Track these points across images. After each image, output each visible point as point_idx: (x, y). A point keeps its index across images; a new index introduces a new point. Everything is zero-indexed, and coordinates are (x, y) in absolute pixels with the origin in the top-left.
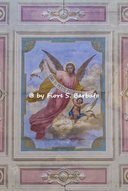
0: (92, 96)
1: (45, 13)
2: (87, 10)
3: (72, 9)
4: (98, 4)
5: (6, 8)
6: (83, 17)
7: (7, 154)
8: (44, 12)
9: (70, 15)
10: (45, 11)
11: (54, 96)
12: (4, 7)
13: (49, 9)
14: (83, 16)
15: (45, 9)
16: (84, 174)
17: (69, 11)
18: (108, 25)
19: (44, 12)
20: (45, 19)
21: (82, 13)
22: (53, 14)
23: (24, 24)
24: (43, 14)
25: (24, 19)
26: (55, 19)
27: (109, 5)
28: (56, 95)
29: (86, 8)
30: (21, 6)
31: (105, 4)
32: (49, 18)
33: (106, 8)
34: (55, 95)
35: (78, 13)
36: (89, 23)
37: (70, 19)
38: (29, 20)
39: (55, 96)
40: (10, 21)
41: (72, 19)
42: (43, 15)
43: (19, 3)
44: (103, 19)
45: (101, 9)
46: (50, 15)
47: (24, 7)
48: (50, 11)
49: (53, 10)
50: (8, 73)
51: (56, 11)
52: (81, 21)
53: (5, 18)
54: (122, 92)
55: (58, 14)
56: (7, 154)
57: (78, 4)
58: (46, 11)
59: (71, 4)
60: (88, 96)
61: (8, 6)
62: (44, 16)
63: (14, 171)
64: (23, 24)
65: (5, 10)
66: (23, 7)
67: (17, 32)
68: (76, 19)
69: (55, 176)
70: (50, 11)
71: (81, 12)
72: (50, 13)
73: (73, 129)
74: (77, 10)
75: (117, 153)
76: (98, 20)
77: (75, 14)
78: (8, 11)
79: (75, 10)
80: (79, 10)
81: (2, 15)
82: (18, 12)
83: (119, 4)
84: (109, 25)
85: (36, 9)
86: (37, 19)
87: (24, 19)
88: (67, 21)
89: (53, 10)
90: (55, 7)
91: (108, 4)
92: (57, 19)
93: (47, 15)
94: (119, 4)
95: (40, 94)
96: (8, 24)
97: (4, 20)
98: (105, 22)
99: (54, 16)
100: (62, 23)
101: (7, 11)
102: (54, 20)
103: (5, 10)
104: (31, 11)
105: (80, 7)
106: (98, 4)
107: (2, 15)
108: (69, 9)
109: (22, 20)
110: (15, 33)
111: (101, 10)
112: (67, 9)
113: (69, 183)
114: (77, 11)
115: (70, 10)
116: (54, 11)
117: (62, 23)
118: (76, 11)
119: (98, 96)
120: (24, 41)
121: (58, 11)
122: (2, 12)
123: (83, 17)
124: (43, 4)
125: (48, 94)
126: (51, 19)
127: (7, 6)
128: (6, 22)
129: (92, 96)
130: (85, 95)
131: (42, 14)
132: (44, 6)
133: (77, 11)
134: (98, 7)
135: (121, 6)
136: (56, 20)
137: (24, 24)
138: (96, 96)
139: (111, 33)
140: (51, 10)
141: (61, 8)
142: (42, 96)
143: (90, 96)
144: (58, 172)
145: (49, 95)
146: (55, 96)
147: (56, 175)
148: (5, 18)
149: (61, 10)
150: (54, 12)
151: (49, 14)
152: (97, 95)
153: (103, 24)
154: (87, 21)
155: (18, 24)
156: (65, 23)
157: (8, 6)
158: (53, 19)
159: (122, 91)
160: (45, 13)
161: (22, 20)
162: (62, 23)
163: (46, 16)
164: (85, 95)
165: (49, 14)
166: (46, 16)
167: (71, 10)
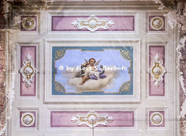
0: (120, 69)
1: (74, 118)
2: (116, 116)
3: (101, 114)
4: (126, 109)
5: (35, 113)
6: (112, 122)
7: (39, 97)
8: (73, 117)
9: (99, 120)
10: (74, 116)
11: (83, 69)
12: (34, 113)
13: (78, 115)
14: (112, 121)
15: (74, 114)
16: (111, 117)
17: (98, 116)
18: (136, 130)
19: (73, 117)
20: (74, 124)
21: (110, 118)
22: (82, 119)
23: (54, 130)
24: (72, 119)
25: (53, 124)
26: (83, 124)
27: (137, 110)
28: (85, 68)
29: (115, 113)
30: (51, 112)
31: (133, 109)
32: (79, 124)
33: (134, 113)
34: (84, 67)
35: (107, 118)
36: (117, 129)
37: (99, 124)
38: (59, 126)
39: (84, 69)
40: (40, 127)
41: (101, 124)
42: (72, 121)
43: (48, 109)
44: (132, 124)
45: (129, 114)
46: (79, 120)
47: (54, 113)
48: (79, 116)
49: (83, 115)
50: (39, 59)
51: (84, 116)
52: (109, 126)
53: (34, 124)
54: (150, 69)
55: (87, 119)
56: (39, 97)
57: (107, 109)
58: (75, 117)
59: (100, 109)
60: (117, 69)
61: (38, 111)
62: (73, 121)
63: (45, 113)
64: (52, 130)
65: (35, 116)
66: (53, 112)
67: (48, 41)
68: (105, 124)
69: (84, 119)
70: (79, 116)
71: (110, 117)
72: (79, 118)
73: (101, 89)
74: (105, 115)
75: (143, 97)
76: (126, 125)
77: (103, 119)
78: (38, 117)
79: (103, 115)
80: (108, 115)
81: (32, 120)
82: (48, 118)
83: (147, 109)
84: (137, 130)
85: (65, 114)
86: (66, 124)
87: (53, 124)
88: (95, 126)
89: (81, 115)
90: (84, 112)
91: (136, 109)
92: (86, 124)
93: (76, 121)
94: (147, 109)
95: (70, 66)
96: (38, 129)
97: (34, 126)
98: (133, 127)
99: (83, 121)
100: (90, 128)
101: (36, 116)
102: (83, 125)
103: (35, 116)
104: (60, 116)
105: (108, 112)
106: (126, 109)
107: (32, 120)
108: (98, 114)
109: (52, 126)
110: (46, 42)
111: (130, 116)
112: (96, 115)
113: (97, 126)
114: (106, 116)
115: (98, 115)
116: (82, 116)
117: (90, 128)
118: (105, 117)
119: (125, 69)
120: (55, 49)
121: (87, 116)
122: (32, 117)
123: (112, 122)
124: (72, 109)
125: (77, 66)
126: (80, 124)
127: (36, 111)
128: (36, 128)
129: (120, 69)
130: (113, 67)
131: (71, 119)
132: (73, 111)
133: (106, 116)
134: (126, 112)
135: (149, 111)
136: (85, 126)
137: (54, 130)
138: (124, 69)
139: (139, 42)
140: (80, 116)
141: (90, 114)
142: (72, 68)
143: (118, 68)
144: (86, 115)
145: (78, 67)
146: (84, 69)
147: (85, 118)
148: (34, 124)
149: (90, 115)
150: (83, 118)
151: (78, 119)
152: (125, 68)
153: (131, 129)
154: (116, 126)
155: (48, 130)
156: (94, 32)
157: (38, 111)
158: (82, 124)
159: (149, 68)
160: (74, 118)
161: (52, 126)
162: (91, 32)
163: (75, 122)
164: (113, 67)
165: (78, 119)
166: (75, 122)
167: (100, 115)
